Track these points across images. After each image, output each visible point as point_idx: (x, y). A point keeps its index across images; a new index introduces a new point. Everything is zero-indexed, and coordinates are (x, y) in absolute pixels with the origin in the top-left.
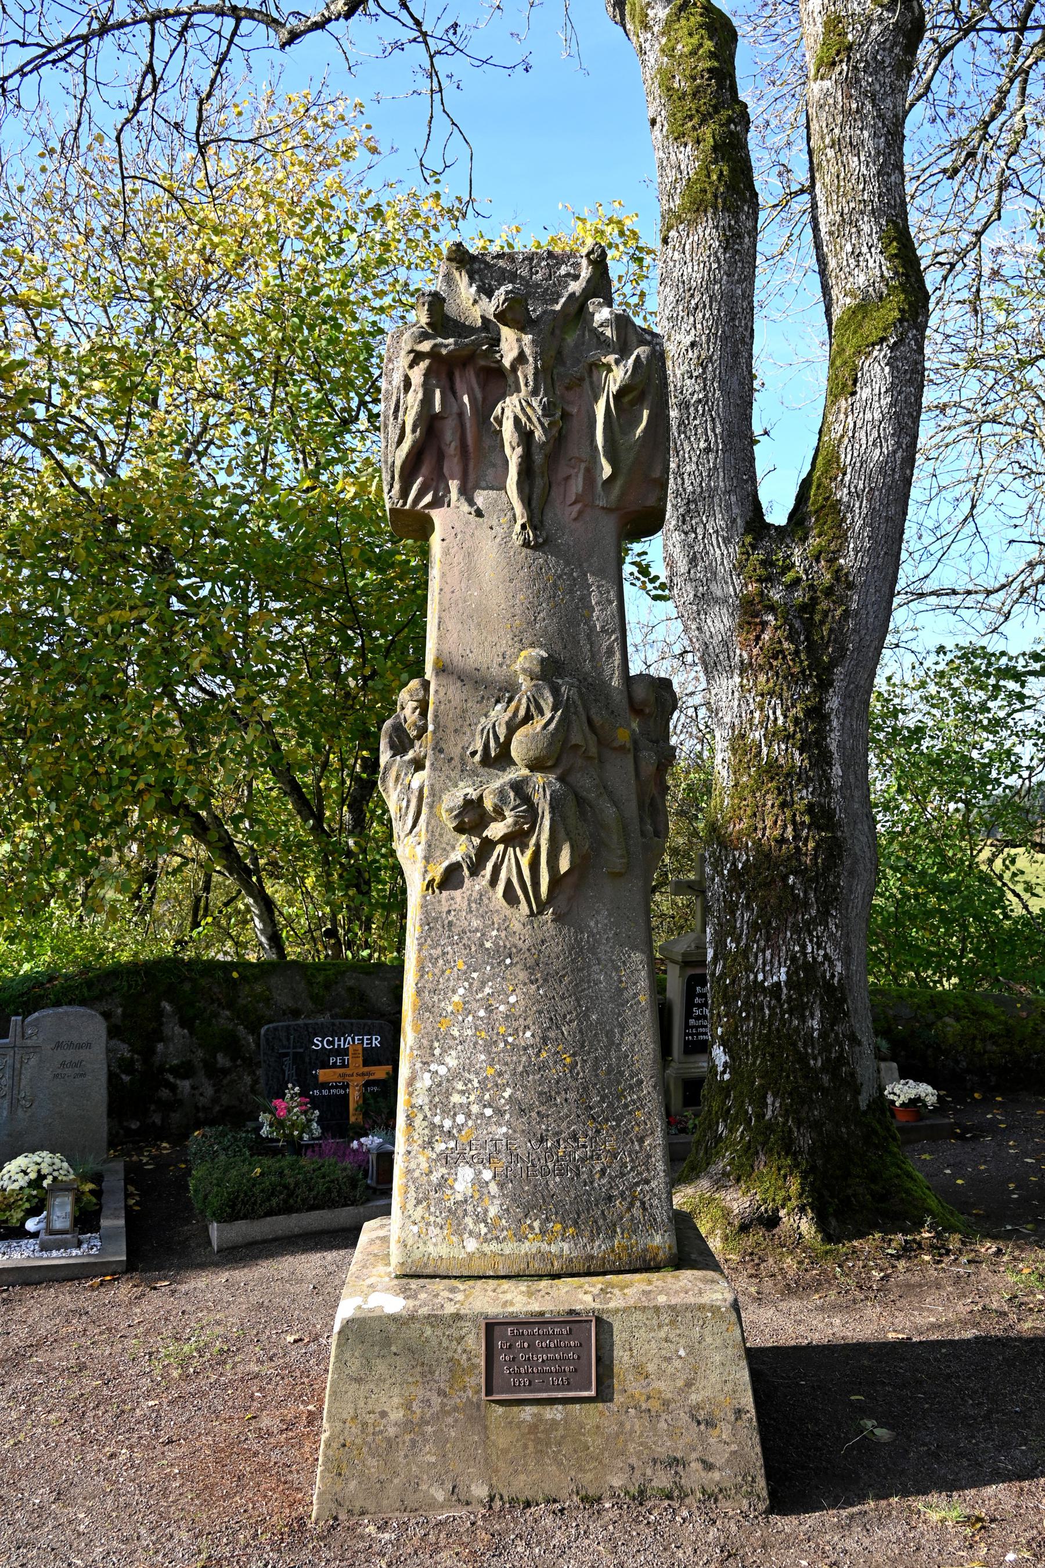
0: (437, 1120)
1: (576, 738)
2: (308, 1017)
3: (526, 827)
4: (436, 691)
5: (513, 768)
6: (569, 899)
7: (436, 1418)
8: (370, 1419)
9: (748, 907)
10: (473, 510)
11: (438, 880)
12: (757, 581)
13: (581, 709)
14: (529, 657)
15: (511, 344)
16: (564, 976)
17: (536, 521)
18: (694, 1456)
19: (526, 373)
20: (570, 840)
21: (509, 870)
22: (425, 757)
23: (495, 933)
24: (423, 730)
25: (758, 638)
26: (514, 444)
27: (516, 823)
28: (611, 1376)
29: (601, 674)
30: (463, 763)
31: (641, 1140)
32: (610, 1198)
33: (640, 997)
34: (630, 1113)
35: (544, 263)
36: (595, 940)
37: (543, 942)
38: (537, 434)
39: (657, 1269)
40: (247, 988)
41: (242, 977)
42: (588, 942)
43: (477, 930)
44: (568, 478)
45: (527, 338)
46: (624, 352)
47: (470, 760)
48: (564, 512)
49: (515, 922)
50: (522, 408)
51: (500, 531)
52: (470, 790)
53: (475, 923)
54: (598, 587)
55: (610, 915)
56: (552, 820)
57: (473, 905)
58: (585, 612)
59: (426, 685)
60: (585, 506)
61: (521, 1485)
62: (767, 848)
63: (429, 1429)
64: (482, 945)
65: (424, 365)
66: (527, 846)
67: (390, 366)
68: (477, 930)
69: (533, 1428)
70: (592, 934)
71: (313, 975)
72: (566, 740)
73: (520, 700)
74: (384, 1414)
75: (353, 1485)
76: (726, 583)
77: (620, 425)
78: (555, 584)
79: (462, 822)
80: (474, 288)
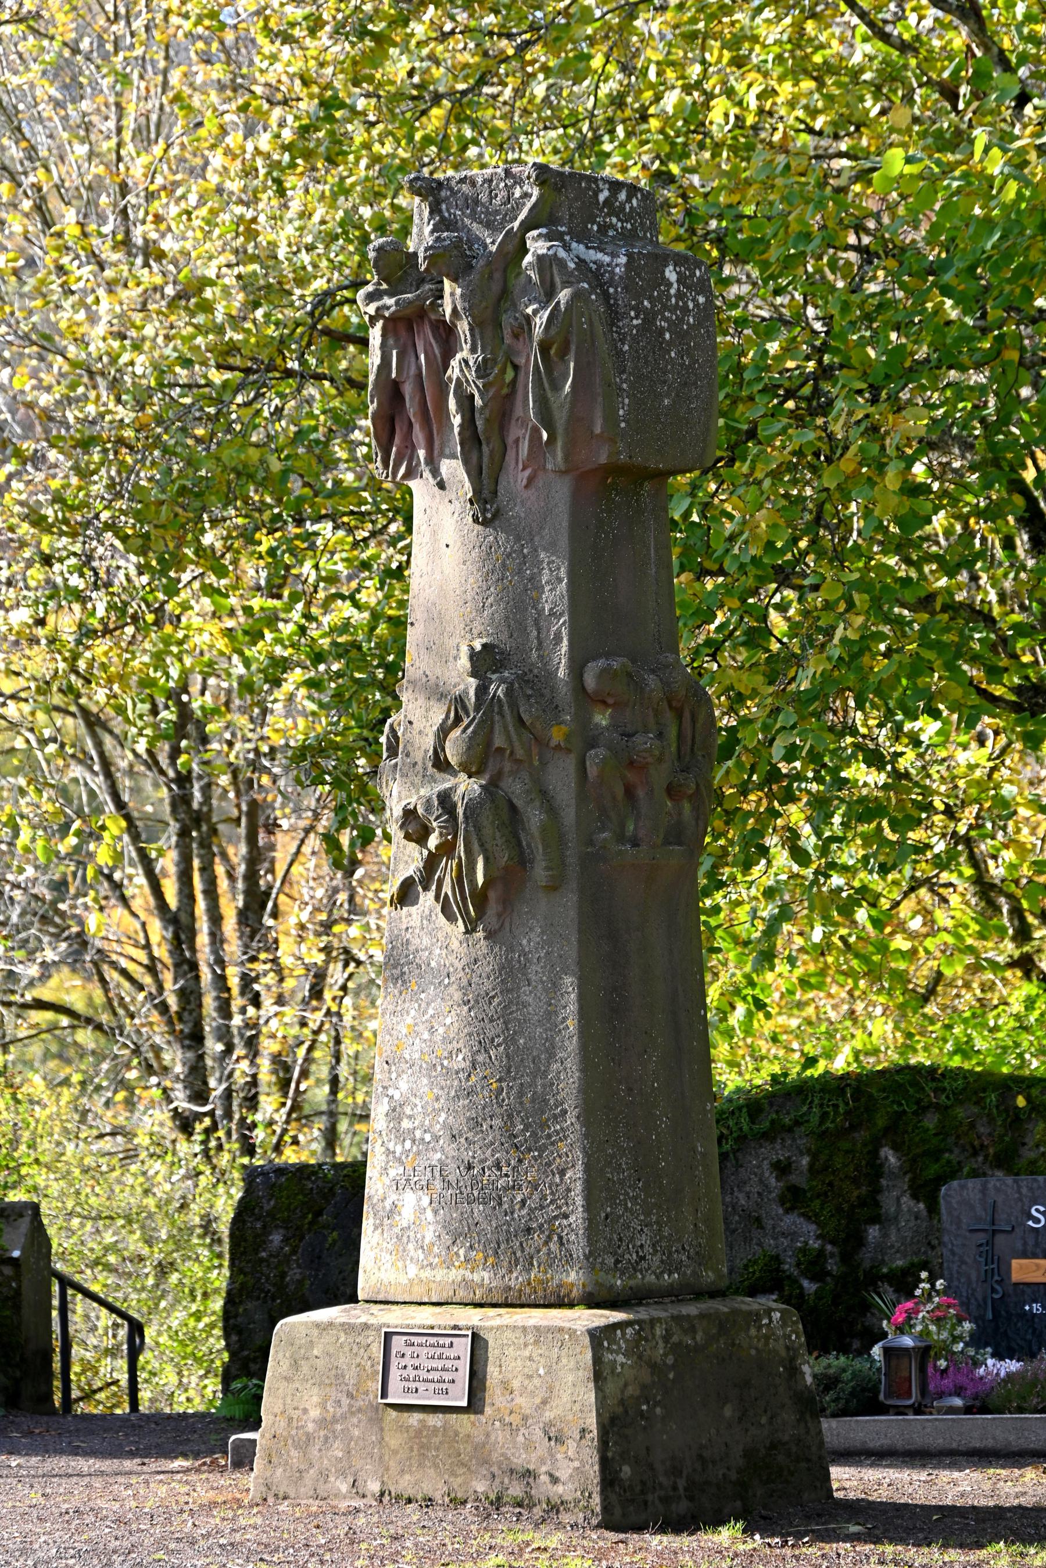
0: (391, 1146)
6: (499, 915)
7: (344, 1417)
8: (295, 1414)
17: (486, 494)
18: (544, 1469)
28: (484, 1389)
31: (562, 1173)
32: (529, 1230)
33: (569, 1022)
34: (553, 1144)
39: (571, 1305)
55: (543, 933)
61: (405, 1484)
63: (339, 1427)
69: (419, 1433)
72: (489, 743)
74: (305, 1411)
75: (279, 1471)
78: (504, 565)
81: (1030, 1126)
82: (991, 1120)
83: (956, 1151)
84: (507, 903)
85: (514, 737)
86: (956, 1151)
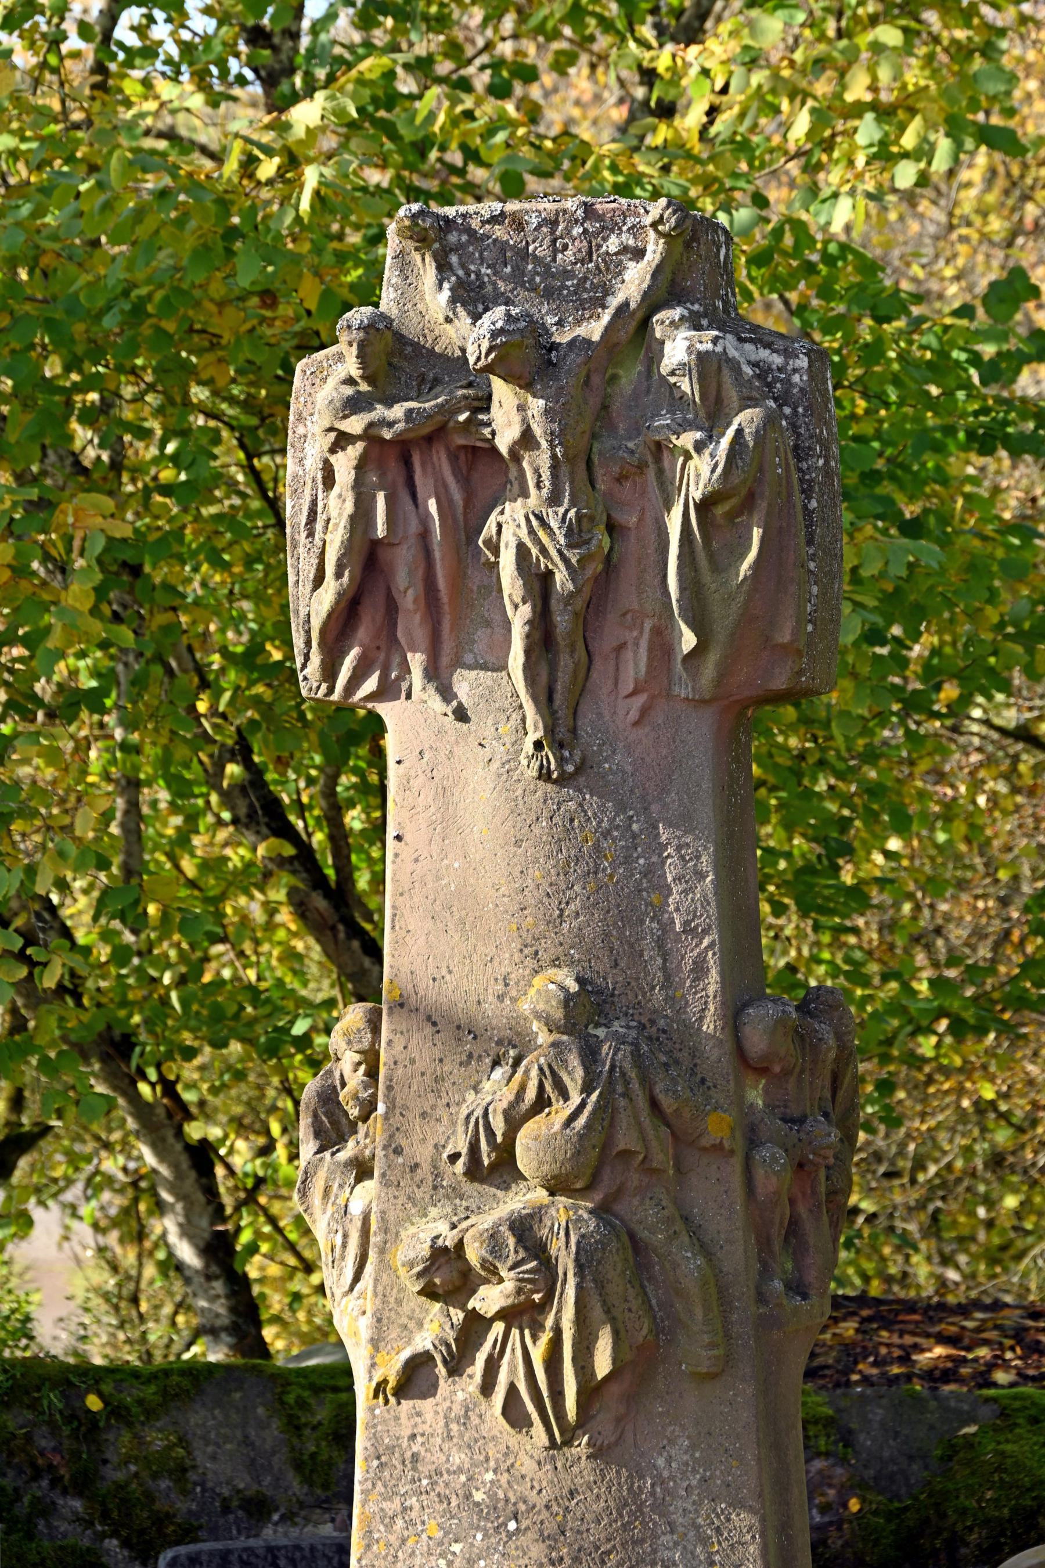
1: (625, 1140)
2: (288, 1518)
3: (537, 1297)
4: (390, 1043)
5: (522, 1184)
6: (618, 1420)
10: (449, 710)
13: (635, 1085)
14: (543, 991)
15: (509, 414)
16: (608, 1553)
17: (562, 733)
19: (538, 462)
20: (613, 1321)
21: (513, 1370)
23: (489, 1476)
24: (368, 1109)
26: (518, 599)
27: (519, 1291)
35: (577, 230)
36: (667, 1491)
37: (572, 1493)
38: (558, 577)
40: (126, 1437)
41: (115, 1411)
42: (653, 1493)
44: (621, 648)
45: (537, 405)
46: (712, 419)
47: (448, 1169)
48: (615, 707)
49: (523, 1458)
50: (531, 532)
51: (500, 751)
53: (458, 1458)
54: (679, 848)
55: (693, 1447)
56: (579, 1287)
57: (454, 1427)
58: (655, 898)
60: (652, 697)
64: (468, 1496)
65: (354, 451)
67: (301, 430)
68: (460, 1470)
70: (659, 1480)
71: (302, 1404)
72: (606, 1145)
73: (527, 1072)
77: (711, 556)
78: (597, 848)
80: (446, 294)
81: (111, 1437)
82: (54, 1429)
83: (11, 1473)
84: (631, 1399)
85: (651, 1133)
86: (11, 1473)
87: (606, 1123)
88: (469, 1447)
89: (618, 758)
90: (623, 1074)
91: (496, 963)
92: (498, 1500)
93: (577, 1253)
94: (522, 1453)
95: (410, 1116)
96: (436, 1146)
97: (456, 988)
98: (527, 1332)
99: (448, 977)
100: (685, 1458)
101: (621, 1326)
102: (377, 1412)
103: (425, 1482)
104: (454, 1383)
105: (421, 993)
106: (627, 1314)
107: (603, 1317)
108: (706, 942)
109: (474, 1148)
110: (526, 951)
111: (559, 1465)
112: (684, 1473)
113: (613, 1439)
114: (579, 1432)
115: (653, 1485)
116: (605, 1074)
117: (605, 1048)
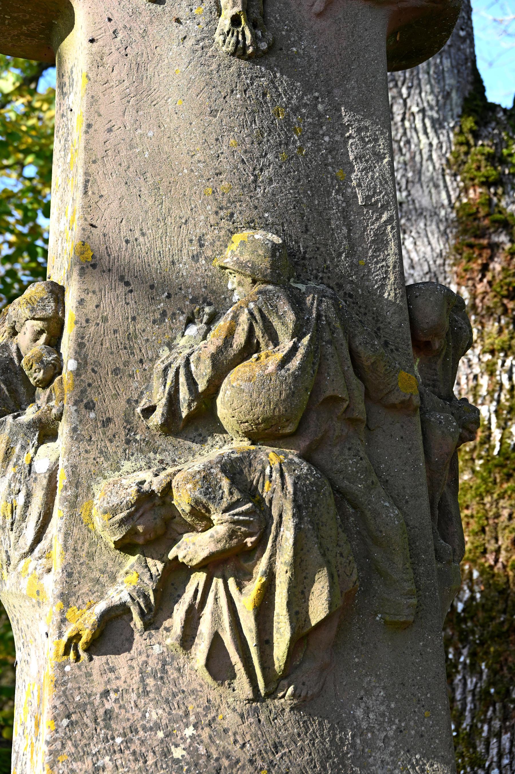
1: (334, 386)
3: (249, 541)
4: (81, 302)
5: (218, 437)
9: (473, 668)
11: (86, 636)
12: (482, 184)
13: (340, 335)
14: (245, 247)
17: (256, 13)
20: (328, 564)
21: (216, 618)
22: (59, 417)
23: (189, 731)
24: (55, 369)
25: (485, 268)
27: (232, 534)
29: (365, 278)
30: (130, 428)
37: (276, 747)
42: (353, 745)
43: (157, 726)
52: (147, 475)
53: (154, 714)
54: (359, 130)
55: (389, 697)
56: (297, 528)
57: (151, 682)
58: (339, 172)
59: (58, 292)
62: (502, 580)
64: (166, 753)
66: (249, 576)
68: (157, 726)
70: (359, 732)
72: (316, 389)
73: (235, 317)
76: (436, 186)
78: (287, 121)
79: (133, 533)
87: (316, 367)
88: (167, 701)
89: (304, 43)
90: (329, 323)
91: (190, 225)
92: (199, 756)
93: (295, 494)
94: (224, 706)
95: (102, 372)
96: (129, 401)
97: (150, 250)
98: (231, 582)
99: (141, 239)
100: (382, 708)
101: (334, 570)
102: (67, 668)
103: (119, 740)
104: (150, 636)
105: (114, 254)
106: (339, 559)
107: (320, 559)
108: (385, 217)
109: (173, 399)
110: (222, 213)
111: (262, 718)
112: (381, 724)
113: (316, 690)
114: (285, 682)
115: (353, 736)
116: (313, 322)
117: (309, 299)
